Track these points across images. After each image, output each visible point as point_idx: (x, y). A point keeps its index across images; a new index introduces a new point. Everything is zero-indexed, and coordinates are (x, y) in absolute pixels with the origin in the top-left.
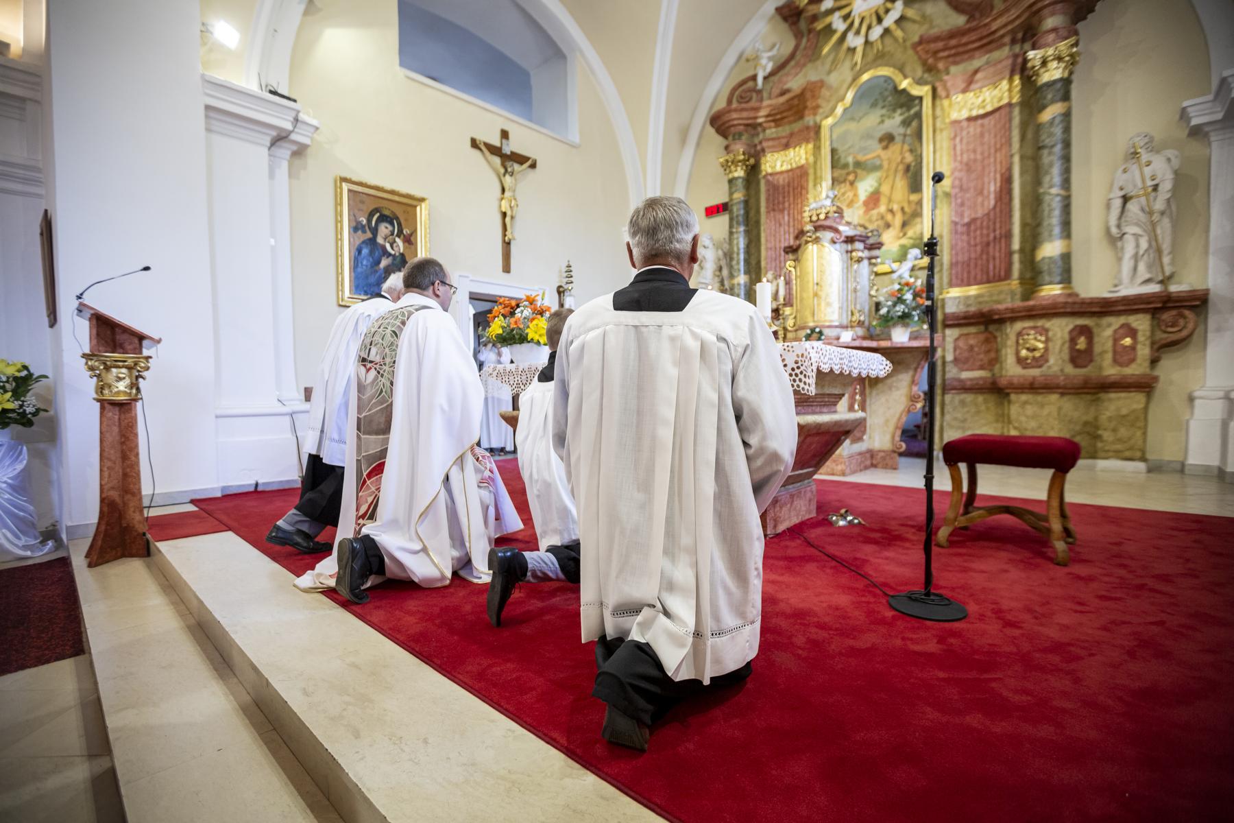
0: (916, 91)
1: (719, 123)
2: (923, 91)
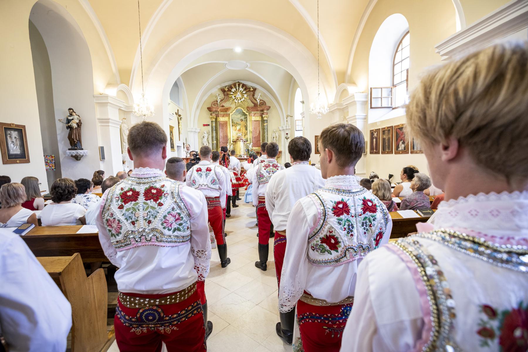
1: (209, 109)
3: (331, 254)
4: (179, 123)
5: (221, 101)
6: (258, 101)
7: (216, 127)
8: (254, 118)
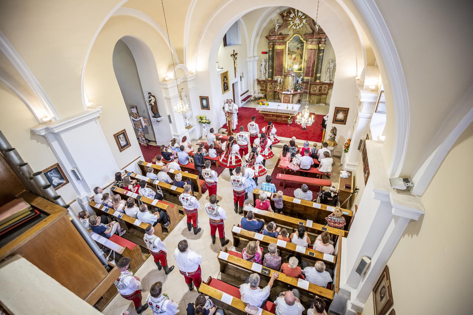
2: (305, 41)
4: (235, 63)
5: (280, 27)
8: (310, 47)
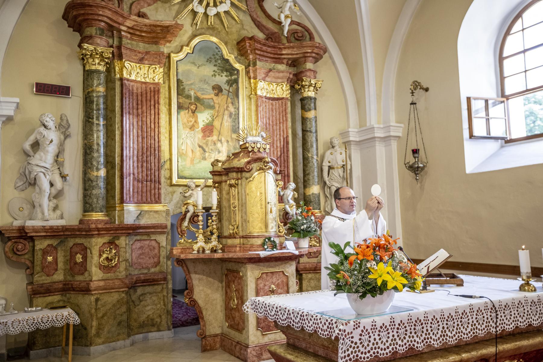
0: (237, 66)
3: (461, 284)
6: (286, 23)
7: (109, 98)
8: (264, 88)
